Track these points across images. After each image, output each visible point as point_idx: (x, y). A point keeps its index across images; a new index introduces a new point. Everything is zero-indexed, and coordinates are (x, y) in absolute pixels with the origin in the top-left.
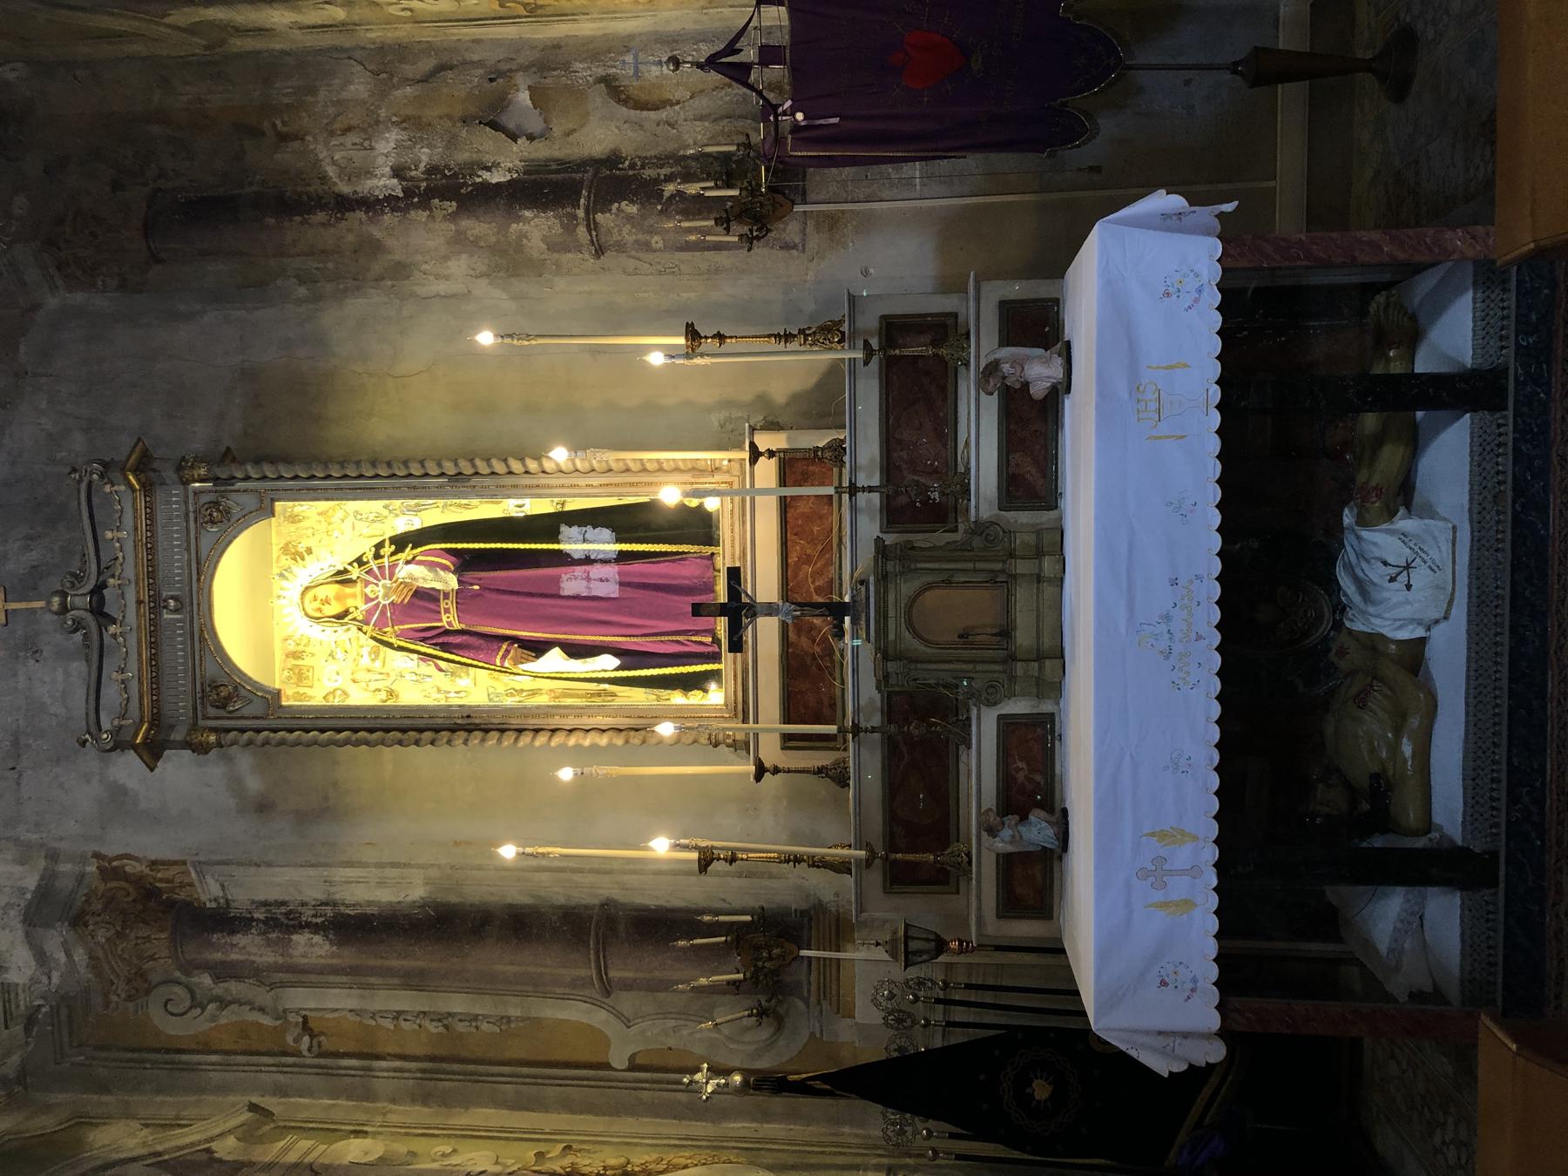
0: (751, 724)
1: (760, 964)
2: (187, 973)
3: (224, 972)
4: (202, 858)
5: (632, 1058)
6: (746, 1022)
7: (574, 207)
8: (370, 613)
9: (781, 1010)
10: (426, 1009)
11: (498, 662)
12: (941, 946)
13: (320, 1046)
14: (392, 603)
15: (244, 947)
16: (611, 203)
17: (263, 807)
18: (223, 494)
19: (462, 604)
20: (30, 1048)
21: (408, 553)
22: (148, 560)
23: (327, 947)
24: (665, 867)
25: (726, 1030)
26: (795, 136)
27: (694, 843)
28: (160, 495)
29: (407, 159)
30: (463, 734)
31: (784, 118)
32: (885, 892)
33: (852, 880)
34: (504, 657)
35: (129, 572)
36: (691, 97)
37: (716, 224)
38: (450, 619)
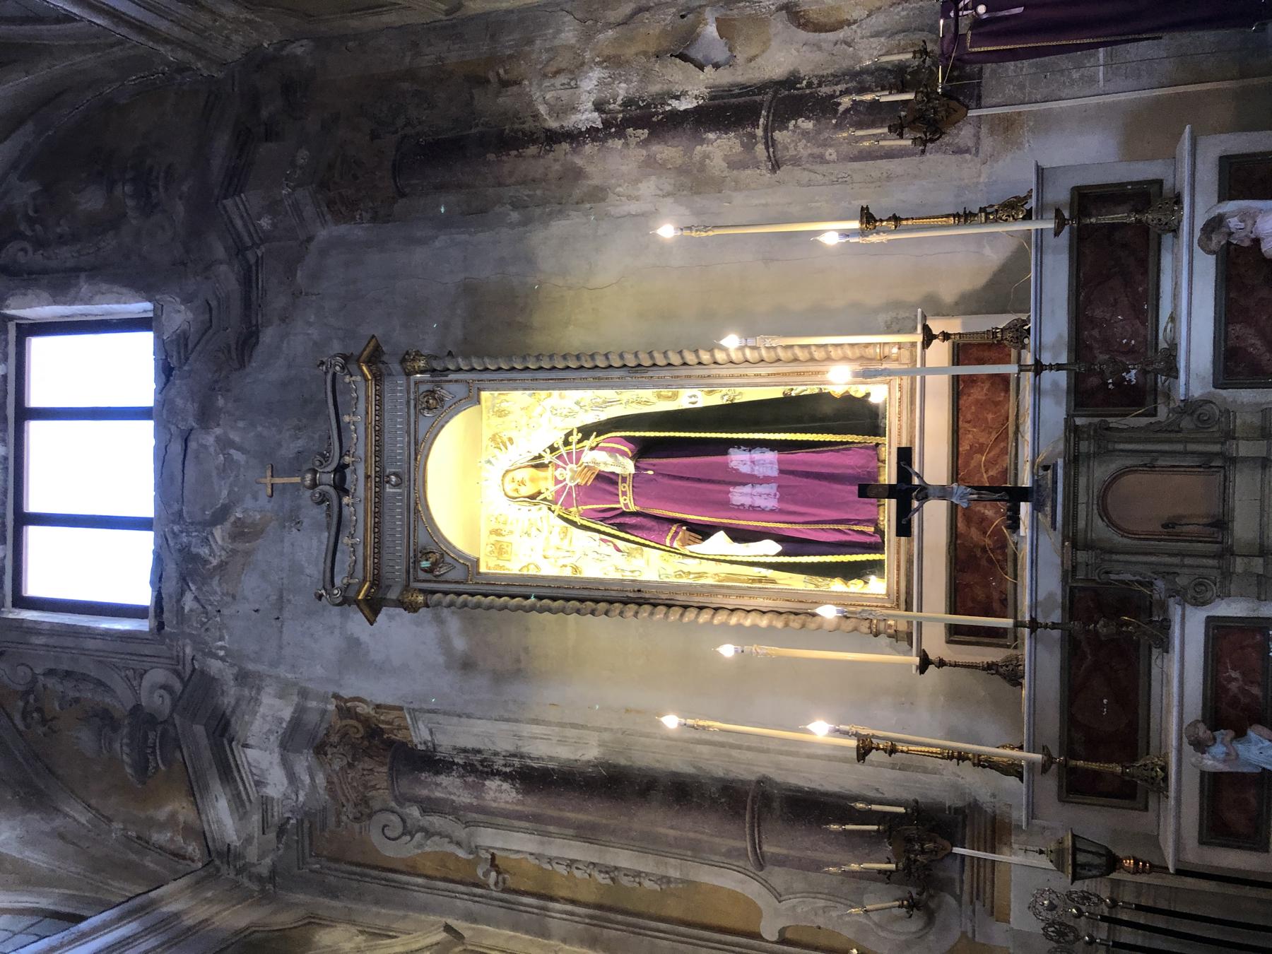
0: (915, 613)
1: (912, 856)
2: (401, 804)
3: (429, 807)
4: (416, 706)
5: (782, 931)
6: (896, 911)
7: (754, 127)
8: (559, 493)
9: (932, 905)
10: (596, 861)
11: (668, 543)
12: (1113, 863)
13: (504, 883)
14: (578, 486)
15: (446, 787)
16: (789, 120)
17: (467, 665)
18: (438, 384)
19: (638, 487)
20: (281, 852)
21: (593, 440)
22: (376, 441)
23: (514, 794)
24: (820, 752)
25: (875, 917)
26: (975, 31)
27: (854, 730)
28: (387, 386)
29: (607, 94)
30: (633, 607)
31: (965, 13)
32: (1061, 800)
33: (1023, 787)
34: (673, 538)
35: (361, 452)
36: (868, 16)
37: (890, 131)
38: (627, 502)
